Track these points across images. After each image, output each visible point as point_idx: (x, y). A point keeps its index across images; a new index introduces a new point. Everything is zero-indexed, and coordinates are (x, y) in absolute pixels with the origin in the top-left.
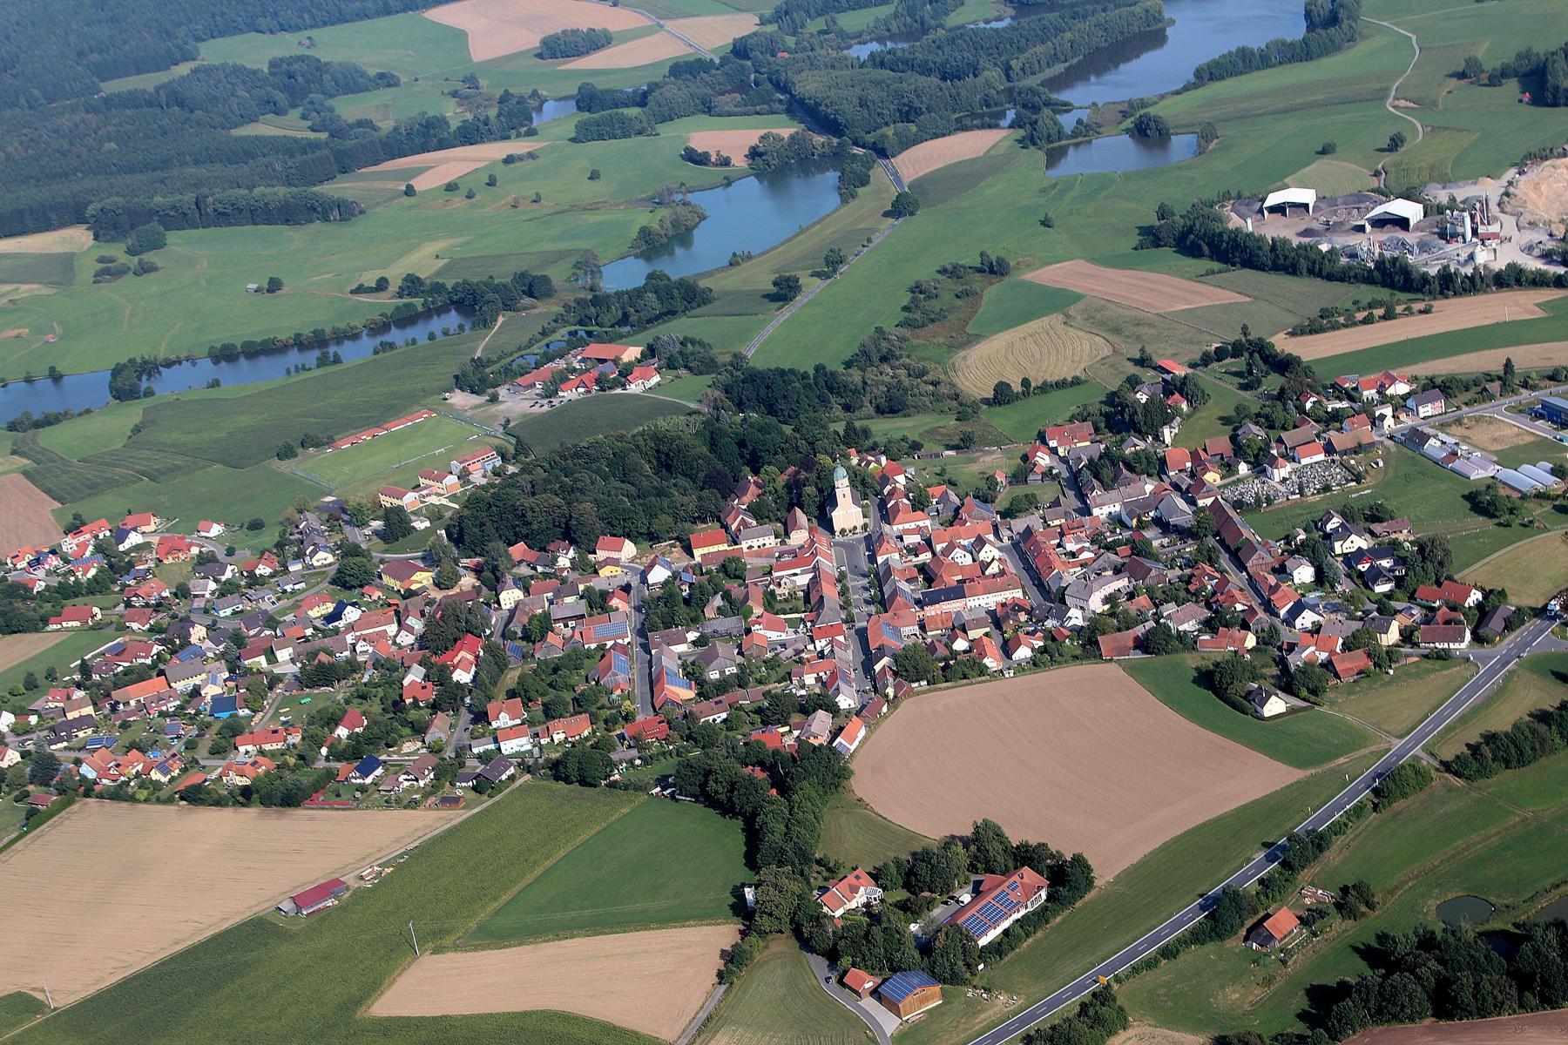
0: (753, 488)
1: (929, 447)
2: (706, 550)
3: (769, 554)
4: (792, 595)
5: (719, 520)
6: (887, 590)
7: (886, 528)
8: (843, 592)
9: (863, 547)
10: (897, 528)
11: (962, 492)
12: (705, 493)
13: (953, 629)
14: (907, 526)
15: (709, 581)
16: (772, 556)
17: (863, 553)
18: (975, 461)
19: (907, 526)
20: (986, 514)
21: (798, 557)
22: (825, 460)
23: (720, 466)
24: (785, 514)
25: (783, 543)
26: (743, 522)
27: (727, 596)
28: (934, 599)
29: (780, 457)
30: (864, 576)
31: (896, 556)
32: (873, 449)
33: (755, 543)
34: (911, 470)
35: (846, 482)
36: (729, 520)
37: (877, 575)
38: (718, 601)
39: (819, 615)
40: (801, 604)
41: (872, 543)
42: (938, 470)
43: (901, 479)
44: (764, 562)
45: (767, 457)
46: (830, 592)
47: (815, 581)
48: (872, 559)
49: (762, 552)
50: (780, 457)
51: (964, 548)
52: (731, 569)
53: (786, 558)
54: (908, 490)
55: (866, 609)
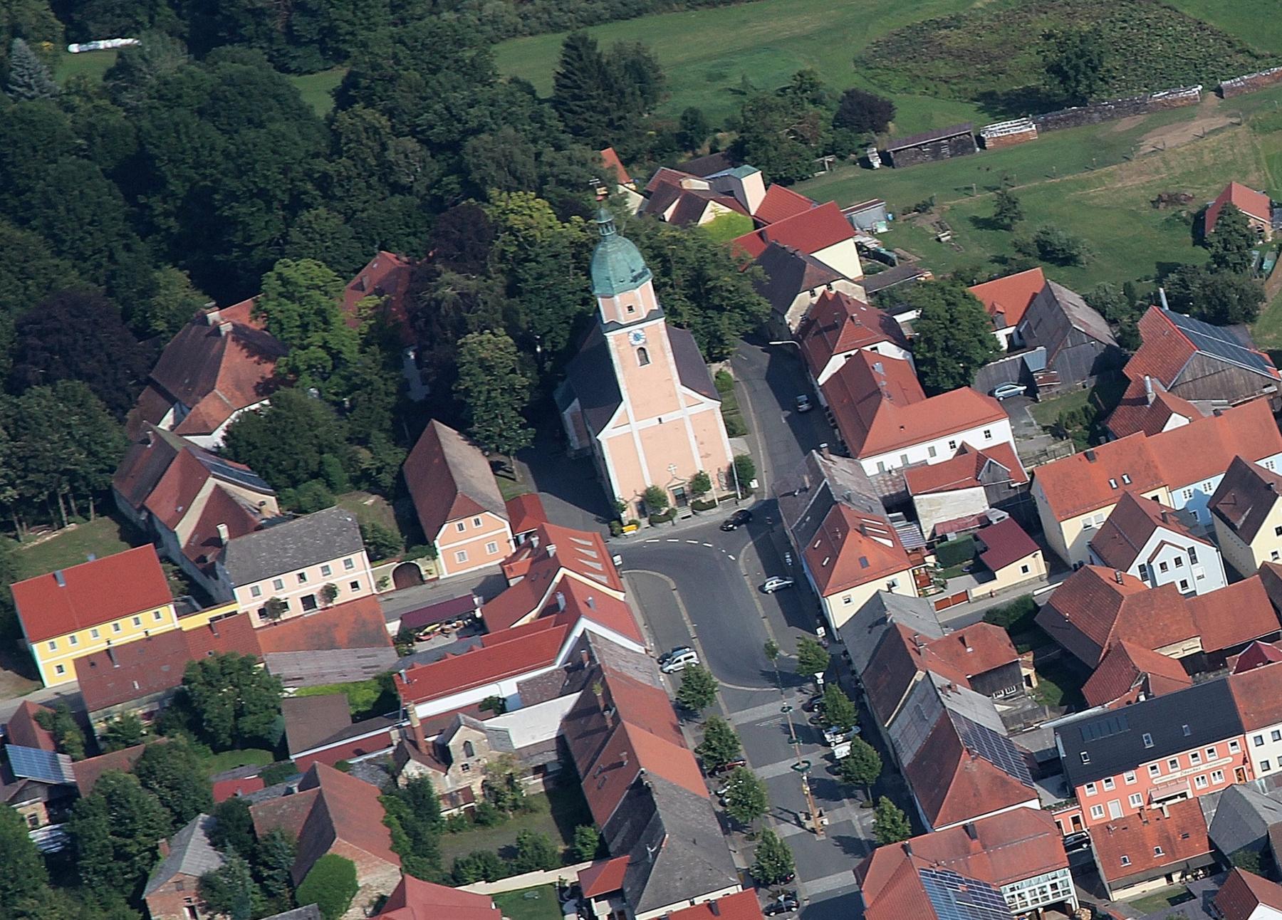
0: (235, 361)
1: (919, 112)
2: (91, 641)
3: (357, 626)
4: (501, 794)
5: (107, 505)
6: (906, 733)
7: (837, 471)
8: (716, 758)
9: (746, 558)
10: (880, 465)
11: (1112, 289)
12: (38, 400)
13: (1218, 865)
14: (917, 454)
15: (146, 773)
16: (378, 638)
17: (753, 586)
18: (1120, 151)
19: (917, 454)
20: (1236, 370)
21: (483, 626)
22: (532, 213)
23: (71, 279)
24: (393, 456)
25: (408, 576)
26: (223, 505)
27: (230, 828)
28: (1117, 751)
29: (322, 217)
30: (786, 680)
31: (905, 583)
32: (686, 138)
33: (291, 589)
34: (874, 219)
35: (645, 297)
36: (160, 502)
37: (839, 668)
38: (196, 855)
39: (642, 870)
40: (543, 827)
41: (789, 538)
42: (982, 204)
43: (842, 258)
44: (350, 668)
45: (262, 225)
46: (667, 762)
47: (594, 724)
48: (802, 606)
49: (328, 624)
50: (322, 217)
51: (1183, 521)
52: (216, 708)
53: (434, 642)
54: (886, 301)
55: (826, 819)
